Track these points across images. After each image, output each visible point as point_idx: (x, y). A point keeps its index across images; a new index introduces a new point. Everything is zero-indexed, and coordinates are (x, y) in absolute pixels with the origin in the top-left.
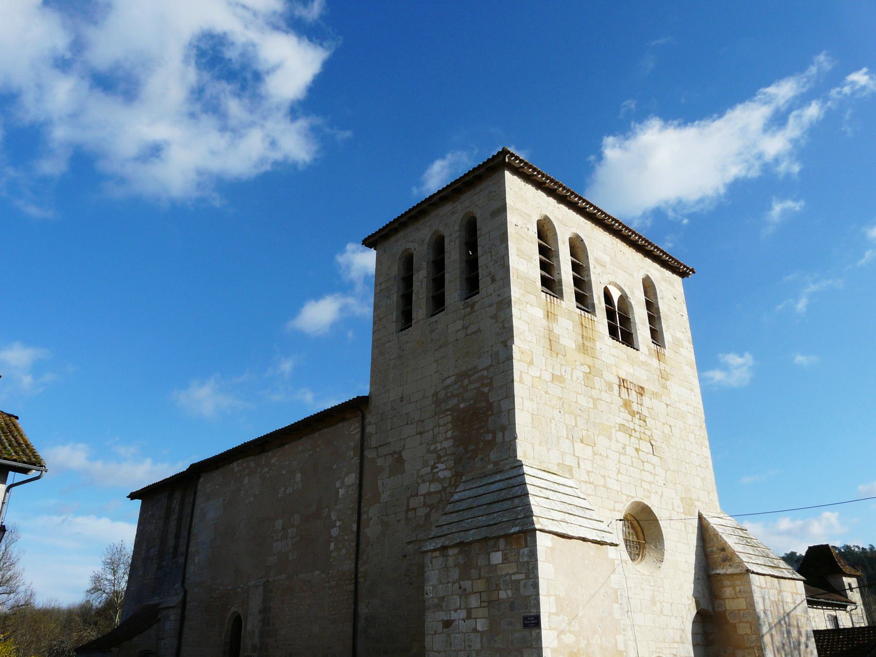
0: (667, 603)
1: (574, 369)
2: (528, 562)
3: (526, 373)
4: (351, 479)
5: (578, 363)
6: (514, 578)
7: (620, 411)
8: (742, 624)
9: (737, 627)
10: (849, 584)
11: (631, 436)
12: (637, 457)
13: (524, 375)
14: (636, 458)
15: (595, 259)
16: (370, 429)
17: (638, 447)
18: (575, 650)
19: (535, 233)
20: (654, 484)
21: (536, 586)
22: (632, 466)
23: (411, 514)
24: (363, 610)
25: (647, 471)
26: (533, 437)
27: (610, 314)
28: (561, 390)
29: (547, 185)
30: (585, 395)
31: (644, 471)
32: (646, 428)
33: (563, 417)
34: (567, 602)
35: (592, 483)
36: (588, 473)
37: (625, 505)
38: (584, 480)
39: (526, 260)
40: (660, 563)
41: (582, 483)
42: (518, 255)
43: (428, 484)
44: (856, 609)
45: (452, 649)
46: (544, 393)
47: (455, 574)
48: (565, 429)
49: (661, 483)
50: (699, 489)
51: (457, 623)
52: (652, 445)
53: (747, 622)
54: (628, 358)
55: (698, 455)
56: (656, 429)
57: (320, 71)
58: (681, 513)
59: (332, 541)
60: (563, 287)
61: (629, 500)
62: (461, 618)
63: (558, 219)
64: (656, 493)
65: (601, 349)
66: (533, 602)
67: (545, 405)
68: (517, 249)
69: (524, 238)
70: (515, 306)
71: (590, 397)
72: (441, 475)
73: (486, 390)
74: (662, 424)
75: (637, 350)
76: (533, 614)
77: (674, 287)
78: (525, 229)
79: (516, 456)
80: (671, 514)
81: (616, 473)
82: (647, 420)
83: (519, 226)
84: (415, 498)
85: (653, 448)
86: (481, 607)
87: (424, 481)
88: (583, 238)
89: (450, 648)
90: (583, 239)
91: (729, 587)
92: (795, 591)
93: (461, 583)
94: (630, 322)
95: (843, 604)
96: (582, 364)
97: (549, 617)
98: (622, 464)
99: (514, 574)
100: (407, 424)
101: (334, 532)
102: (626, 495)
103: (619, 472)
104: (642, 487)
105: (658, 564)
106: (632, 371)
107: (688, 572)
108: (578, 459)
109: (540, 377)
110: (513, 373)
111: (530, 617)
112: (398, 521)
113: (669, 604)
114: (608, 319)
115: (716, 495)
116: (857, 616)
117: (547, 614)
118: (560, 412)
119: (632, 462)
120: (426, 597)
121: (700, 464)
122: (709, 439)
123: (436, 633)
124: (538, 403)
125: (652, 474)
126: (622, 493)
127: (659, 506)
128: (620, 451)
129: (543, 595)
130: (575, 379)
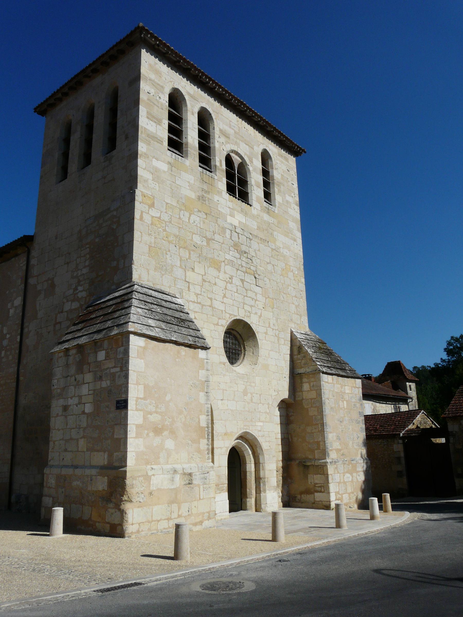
0: (257, 394)
1: (192, 214)
2: (122, 359)
3: (147, 213)
4: (18, 301)
5: (196, 210)
6: (113, 370)
7: (230, 250)
8: (312, 408)
9: (309, 410)
10: (410, 386)
11: (238, 270)
12: (242, 286)
13: (144, 215)
14: (241, 286)
15: (221, 131)
16: (33, 262)
17: (243, 279)
18: (160, 426)
19: (167, 102)
20: (255, 307)
21: (126, 377)
22: (237, 292)
23: (58, 327)
24: (23, 401)
25: (249, 297)
26: (149, 264)
27: (230, 176)
28: (178, 230)
29: (181, 64)
30: (200, 235)
31: (247, 297)
32: (252, 264)
33: (178, 250)
34: (156, 390)
35: (200, 303)
36: (197, 295)
37: (228, 321)
38: (193, 301)
39: (155, 122)
40: (254, 365)
41: (191, 303)
42: (148, 118)
43: (70, 302)
44: (412, 401)
45: (68, 427)
46: (162, 231)
47: (73, 370)
48: (179, 260)
49: (261, 307)
50: (293, 314)
51: (72, 407)
52: (255, 278)
53: (315, 407)
54: (242, 211)
55: (294, 288)
56: (261, 266)
57: (171, 91)
58: (276, 330)
59: (3, 350)
60: (189, 149)
61: (232, 318)
62: (75, 404)
63: (189, 94)
64: (256, 313)
65: (218, 201)
66: (124, 389)
67: (162, 240)
68: (147, 112)
69: (154, 104)
70: (141, 158)
71: (204, 237)
72: (80, 295)
73: (114, 227)
74: (266, 263)
75: (251, 206)
76: (123, 399)
77: (288, 162)
78: (157, 97)
79: (132, 278)
80: (267, 330)
81: (222, 297)
82: (254, 259)
83: (152, 94)
84: (61, 314)
85: (256, 281)
86: (89, 395)
87: (68, 301)
88: (211, 112)
89: (67, 426)
90: (211, 113)
91: (306, 383)
92: (355, 385)
93: (77, 376)
94: (247, 184)
95: (405, 400)
96: (199, 211)
97: (136, 401)
98: (228, 290)
99: (112, 368)
100: (59, 256)
101: (5, 343)
102: (229, 314)
103: (225, 296)
104: (243, 308)
105: (253, 366)
106: (244, 221)
107: (277, 373)
108: (189, 284)
109: (159, 218)
110: (134, 212)
111: (121, 401)
112: (49, 332)
113: (258, 395)
114: (227, 179)
115: (307, 318)
116: (412, 406)
117: (135, 399)
118: (175, 246)
119: (237, 289)
120: (53, 388)
121: (296, 295)
122: (305, 278)
123: (58, 415)
124: (155, 238)
125: (254, 300)
126: (226, 312)
127: (258, 323)
128: (227, 281)
129: (132, 384)
130: (192, 221)
